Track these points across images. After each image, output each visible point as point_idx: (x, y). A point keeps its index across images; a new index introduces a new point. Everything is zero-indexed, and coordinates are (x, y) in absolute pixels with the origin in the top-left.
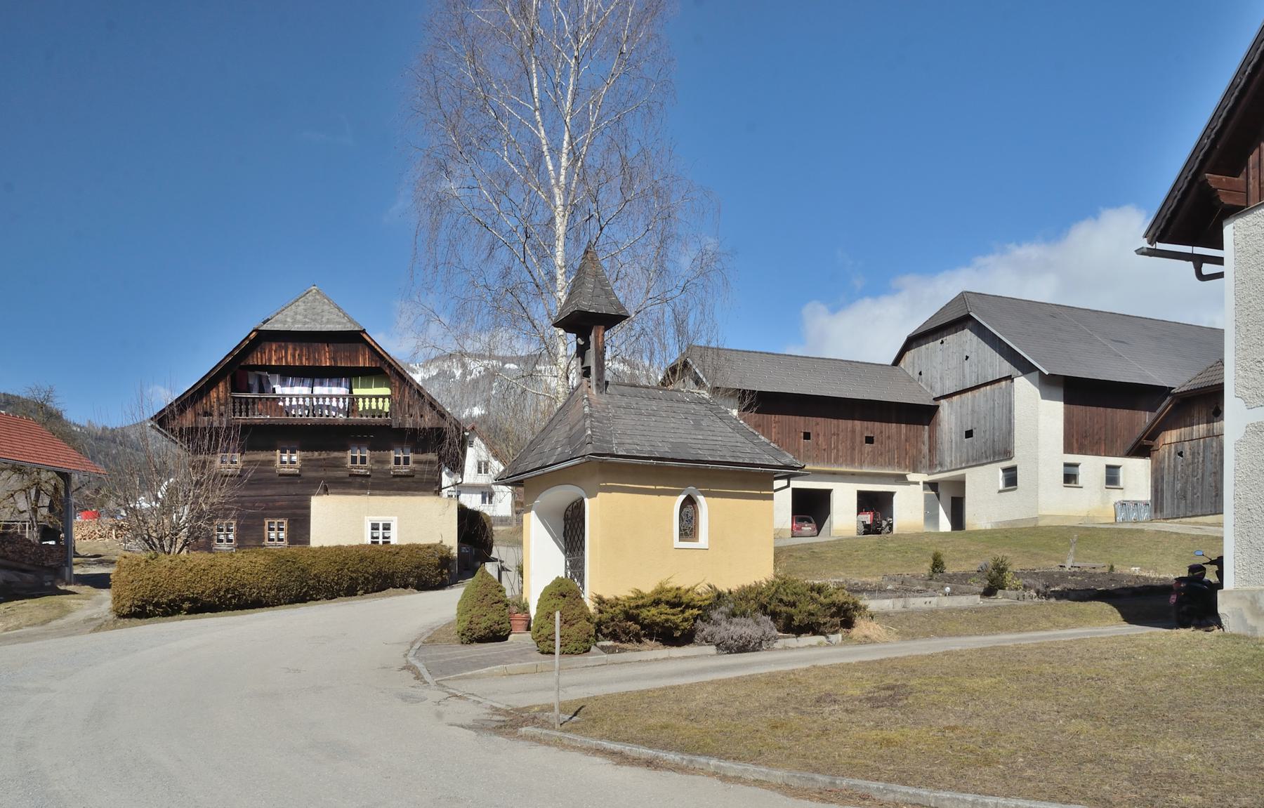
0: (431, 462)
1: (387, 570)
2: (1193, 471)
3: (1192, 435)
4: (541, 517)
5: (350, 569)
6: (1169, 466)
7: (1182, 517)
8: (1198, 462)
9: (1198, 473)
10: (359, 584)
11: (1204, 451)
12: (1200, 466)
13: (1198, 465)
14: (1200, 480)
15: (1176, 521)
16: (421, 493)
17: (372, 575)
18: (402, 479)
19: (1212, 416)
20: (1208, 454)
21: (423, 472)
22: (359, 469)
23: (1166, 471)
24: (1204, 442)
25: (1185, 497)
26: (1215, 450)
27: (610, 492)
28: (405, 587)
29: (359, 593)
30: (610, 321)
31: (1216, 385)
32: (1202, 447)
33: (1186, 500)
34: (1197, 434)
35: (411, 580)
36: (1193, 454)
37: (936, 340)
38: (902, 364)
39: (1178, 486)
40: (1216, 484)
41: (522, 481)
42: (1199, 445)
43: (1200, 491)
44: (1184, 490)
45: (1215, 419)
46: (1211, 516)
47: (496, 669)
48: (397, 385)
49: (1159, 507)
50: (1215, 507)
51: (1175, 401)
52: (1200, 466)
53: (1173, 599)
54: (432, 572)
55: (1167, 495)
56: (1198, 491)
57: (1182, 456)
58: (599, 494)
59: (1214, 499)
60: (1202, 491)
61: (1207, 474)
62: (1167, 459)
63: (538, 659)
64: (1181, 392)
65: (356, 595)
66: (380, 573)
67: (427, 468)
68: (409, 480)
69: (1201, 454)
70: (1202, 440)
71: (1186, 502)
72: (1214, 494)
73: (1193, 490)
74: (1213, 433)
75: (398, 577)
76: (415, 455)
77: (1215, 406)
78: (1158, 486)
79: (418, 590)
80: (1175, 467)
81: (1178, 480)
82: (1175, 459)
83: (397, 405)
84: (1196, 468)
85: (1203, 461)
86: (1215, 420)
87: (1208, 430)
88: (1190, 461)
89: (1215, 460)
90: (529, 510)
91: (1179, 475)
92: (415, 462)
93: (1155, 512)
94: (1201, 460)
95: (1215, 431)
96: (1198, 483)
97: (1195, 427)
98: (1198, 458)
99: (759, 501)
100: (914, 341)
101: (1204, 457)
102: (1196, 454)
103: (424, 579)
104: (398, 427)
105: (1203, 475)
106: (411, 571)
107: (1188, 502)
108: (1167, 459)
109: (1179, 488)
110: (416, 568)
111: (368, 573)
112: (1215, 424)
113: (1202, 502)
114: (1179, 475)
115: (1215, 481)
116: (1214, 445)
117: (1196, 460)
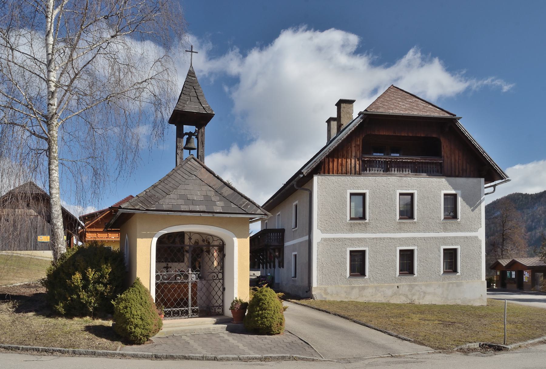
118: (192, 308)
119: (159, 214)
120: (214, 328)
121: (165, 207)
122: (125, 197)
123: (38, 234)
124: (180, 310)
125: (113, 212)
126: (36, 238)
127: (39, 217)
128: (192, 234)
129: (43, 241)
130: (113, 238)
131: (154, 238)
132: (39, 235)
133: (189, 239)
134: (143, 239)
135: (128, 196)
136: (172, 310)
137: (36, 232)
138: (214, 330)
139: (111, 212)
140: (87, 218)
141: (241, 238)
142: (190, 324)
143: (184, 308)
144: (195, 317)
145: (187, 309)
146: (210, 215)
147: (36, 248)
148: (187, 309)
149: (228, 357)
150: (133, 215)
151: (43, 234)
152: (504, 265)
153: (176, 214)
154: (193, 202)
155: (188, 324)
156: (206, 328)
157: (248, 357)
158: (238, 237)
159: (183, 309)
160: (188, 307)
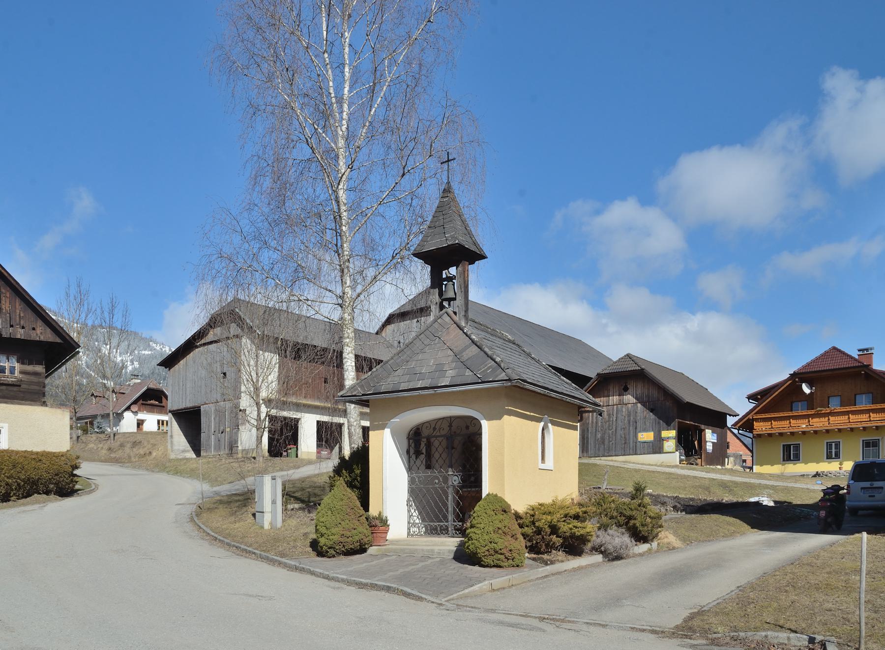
0: (36, 374)
1: (34, 476)
2: (609, 426)
3: (609, 402)
4: (393, 434)
5: (6, 474)
6: (592, 422)
7: (601, 457)
8: (613, 420)
9: (612, 427)
10: (12, 490)
11: (617, 413)
12: (614, 423)
13: (612, 423)
14: (614, 432)
15: (597, 458)
16: (27, 403)
17: (23, 480)
18: (8, 387)
19: (623, 391)
20: (619, 415)
21: (31, 383)
22: (7, 378)
23: (590, 426)
24: (617, 408)
25: (603, 443)
26: (624, 413)
27: (510, 416)
28: (47, 493)
29: (12, 498)
30: (473, 256)
31: (629, 371)
32: (615, 411)
33: (604, 445)
34: (612, 402)
35: (52, 486)
36: (609, 415)
37: (413, 319)
38: (383, 334)
39: (599, 436)
40: (625, 436)
41: (368, 401)
42: (613, 409)
43: (614, 439)
44: (603, 439)
45: (624, 393)
46: (621, 457)
47: (485, 585)
48: (8, 295)
49: (585, 449)
50: (624, 451)
51: (599, 379)
52: (614, 423)
53: (823, 513)
54: (67, 479)
55: (591, 441)
56: (612, 440)
57: (601, 416)
58: (505, 416)
59: (623, 445)
60: (616, 440)
61: (619, 429)
62: (591, 417)
63: (493, 577)
64: (605, 373)
65: (9, 501)
66: (29, 479)
67: (33, 379)
68: (15, 389)
69: (615, 416)
70: (615, 406)
71: (604, 447)
72: (623, 442)
73: (609, 439)
74: (623, 402)
75: (42, 484)
76: (21, 366)
77: (625, 384)
78: (584, 435)
79: (60, 496)
80: (597, 423)
81: (598, 432)
82: (596, 417)
83: (8, 315)
84: (611, 425)
85: (616, 420)
86: (624, 393)
87: (620, 400)
88: (607, 419)
89: (624, 420)
90: (382, 427)
91: (599, 429)
92: (21, 372)
93: (583, 452)
94: (615, 419)
95: (624, 401)
96: (612, 434)
97: (610, 398)
98: (613, 418)
99: (571, 431)
100: (390, 320)
101: (617, 418)
102: (611, 415)
103: (61, 486)
104: (8, 336)
105: (616, 429)
106: (52, 478)
107: (605, 446)
108: (591, 417)
109: (599, 437)
110: (56, 475)
111: (20, 479)
112: (624, 396)
113: (615, 447)
114: (599, 429)
115: (624, 434)
116: (624, 410)
117: (611, 419)
118: (454, 523)
119: (374, 398)
120: (439, 550)
121: (383, 389)
122: (822, 351)
123: (638, 430)
124: (439, 525)
125: (797, 382)
126: (636, 436)
127: (639, 405)
128: (452, 419)
129: (645, 440)
130: (805, 426)
131: (386, 429)
132: (640, 432)
133: (449, 426)
134: (376, 431)
135: (827, 348)
136: (429, 525)
137: (636, 428)
138: (439, 553)
139: (794, 382)
140: (759, 397)
141: (492, 420)
142: (428, 544)
143: (443, 523)
144: (457, 536)
145: (446, 524)
146: (431, 391)
147: (636, 451)
148: (446, 524)
149: (337, 577)
150: (174, 411)
151: (645, 430)
152: (662, 432)
153: (392, 396)
154: (422, 376)
155: (424, 544)
156: (429, 550)
157: (355, 580)
158: (489, 418)
159: (442, 524)
160: (447, 521)
